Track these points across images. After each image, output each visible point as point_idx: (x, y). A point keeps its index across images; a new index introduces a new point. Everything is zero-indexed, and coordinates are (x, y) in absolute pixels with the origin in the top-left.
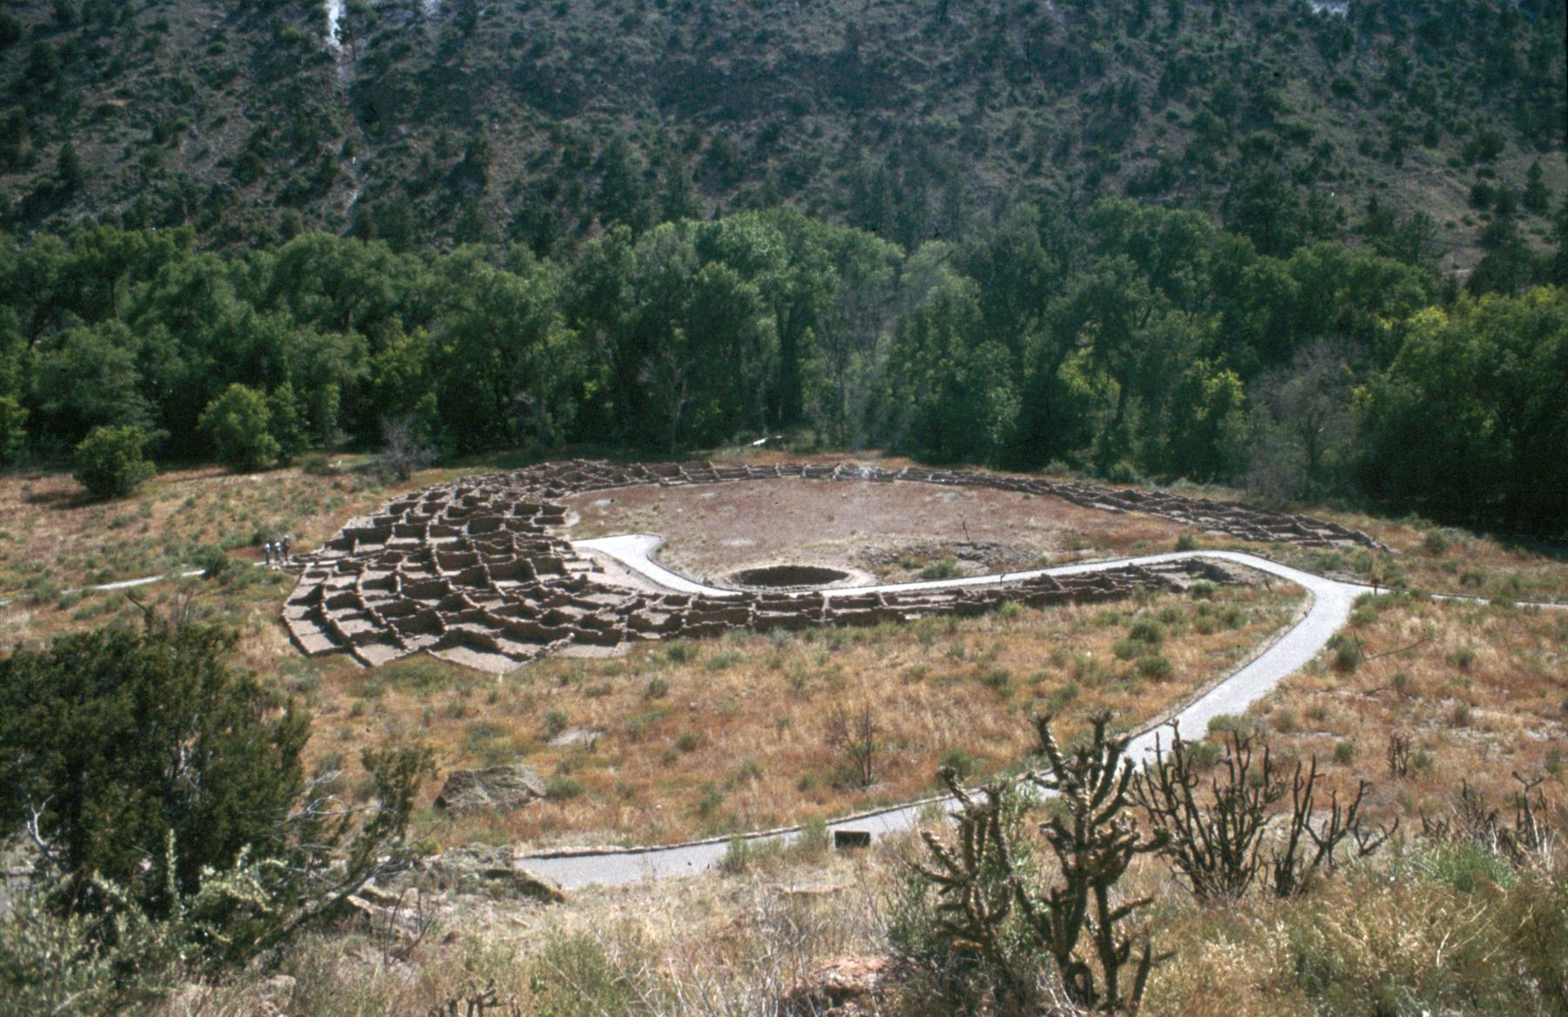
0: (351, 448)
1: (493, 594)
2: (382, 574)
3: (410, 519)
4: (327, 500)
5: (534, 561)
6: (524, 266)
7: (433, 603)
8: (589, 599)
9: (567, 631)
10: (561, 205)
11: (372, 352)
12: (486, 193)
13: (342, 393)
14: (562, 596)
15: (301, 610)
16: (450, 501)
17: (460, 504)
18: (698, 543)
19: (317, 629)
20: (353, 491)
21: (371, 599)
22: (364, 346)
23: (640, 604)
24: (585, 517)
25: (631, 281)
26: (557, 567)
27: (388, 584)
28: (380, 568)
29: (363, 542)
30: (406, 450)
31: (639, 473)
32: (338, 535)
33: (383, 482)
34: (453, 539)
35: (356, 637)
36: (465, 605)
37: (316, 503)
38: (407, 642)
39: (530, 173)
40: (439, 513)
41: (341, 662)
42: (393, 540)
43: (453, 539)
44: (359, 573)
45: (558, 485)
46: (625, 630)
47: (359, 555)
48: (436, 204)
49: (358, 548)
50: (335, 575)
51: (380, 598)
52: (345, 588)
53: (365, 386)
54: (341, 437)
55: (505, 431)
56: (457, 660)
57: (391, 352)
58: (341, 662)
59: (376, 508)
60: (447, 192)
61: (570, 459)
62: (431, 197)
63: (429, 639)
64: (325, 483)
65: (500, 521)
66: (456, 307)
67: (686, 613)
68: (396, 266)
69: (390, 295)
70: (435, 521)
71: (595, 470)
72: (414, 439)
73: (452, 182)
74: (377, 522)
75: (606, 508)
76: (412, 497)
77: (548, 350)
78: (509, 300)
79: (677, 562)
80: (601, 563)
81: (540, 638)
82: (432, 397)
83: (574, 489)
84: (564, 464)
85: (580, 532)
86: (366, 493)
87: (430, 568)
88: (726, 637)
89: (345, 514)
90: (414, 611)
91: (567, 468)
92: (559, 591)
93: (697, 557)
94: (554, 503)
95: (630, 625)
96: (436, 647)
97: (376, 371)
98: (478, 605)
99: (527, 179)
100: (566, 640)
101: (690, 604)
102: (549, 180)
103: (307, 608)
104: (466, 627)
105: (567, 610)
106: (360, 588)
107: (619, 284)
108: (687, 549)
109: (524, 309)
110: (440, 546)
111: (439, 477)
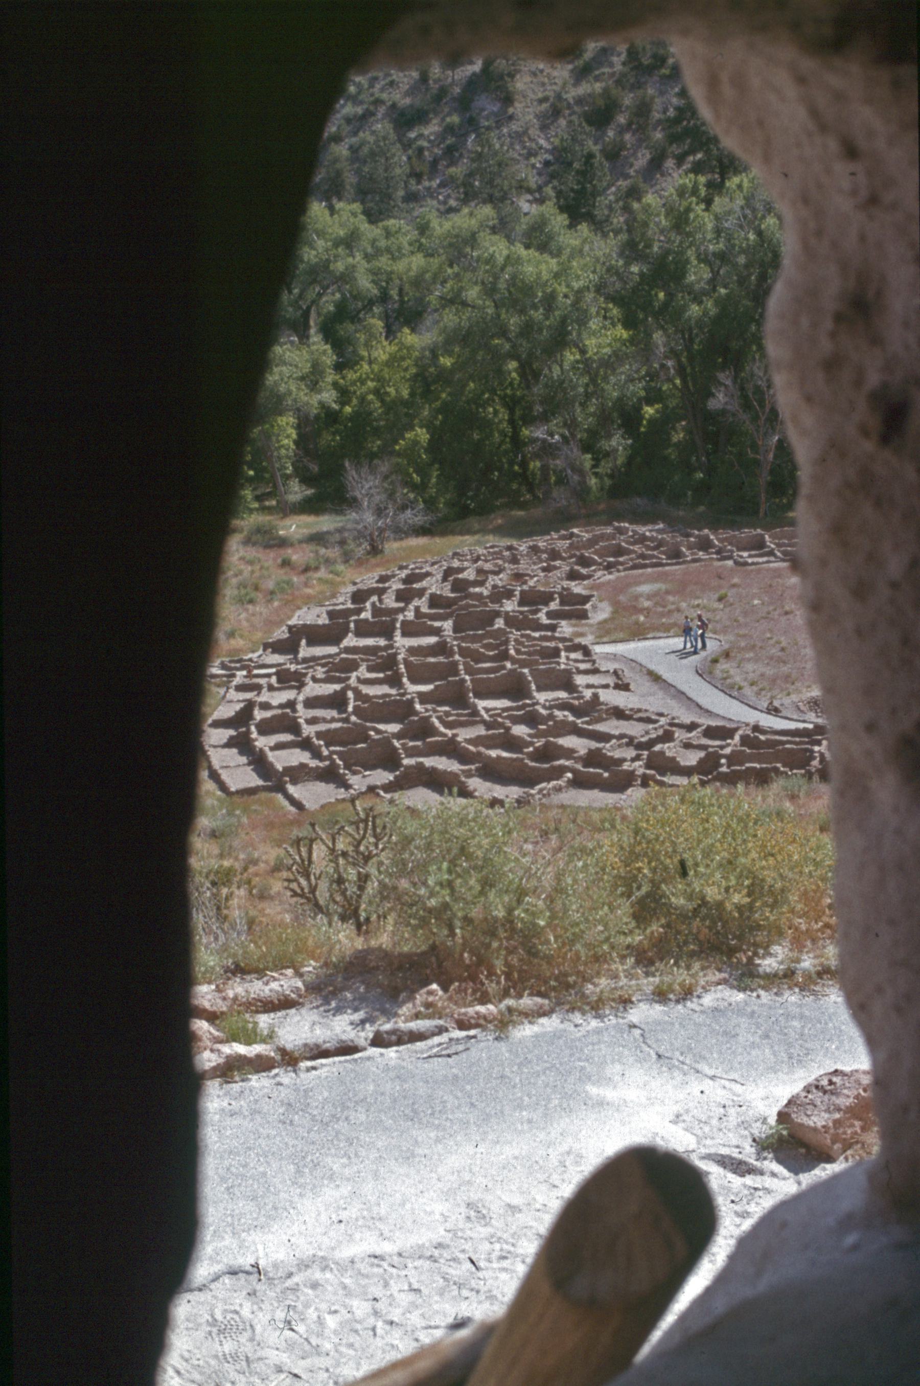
0: (309, 507)
1: (473, 717)
2: (330, 688)
3: (376, 611)
4: (270, 585)
5: (532, 672)
6: (550, 237)
7: (393, 728)
8: (601, 727)
9: (562, 770)
10: (622, 131)
11: (339, 367)
12: (511, 118)
13: (298, 427)
14: (564, 723)
15: (226, 734)
16: (434, 585)
17: (446, 591)
18: (774, 651)
19: (244, 760)
20: (307, 569)
21: (312, 721)
22: (329, 358)
23: (667, 737)
24: (618, 609)
25: (703, 258)
26: (566, 682)
27: (337, 702)
28: (328, 680)
29: (310, 643)
30: (379, 512)
31: (705, 545)
32: (281, 633)
33: (347, 558)
34: (432, 640)
35: (288, 770)
36: (433, 731)
37: (256, 588)
38: (353, 780)
39: (577, 82)
40: (416, 602)
41: (270, 803)
42: (350, 641)
43: (432, 640)
44: (301, 686)
45: (585, 562)
46: (640, 771)
47: (305, 660)
48: (442, 137)
49: (305, 651)
50: (271, 688)
51: (324, 720)
52: (281, 706)
53: (330, 417)
54: (297, 492)
55: (525, 477)
56: (566, 802)
57: (366, 367)
58: (270, 803)
59: (334, 596)
60: (455, 119)
61: (608, 523)
62: (432, 129)
63: (382, 777)
64: (270, 558)
65: (497, 614)
66: (455, 301)
67: (728, 751)
68: (374, 242)
69: (365, 283)
70: (410, 615)
71: (642, 539)
72: (391, 496)
73: (464, 103)
74: (331, 614)
75: (649, 597)
76: (383, 579)
77: (587, 362)
78: (528, 290)
79: (738, 679)
80: (628, 675)
81: (526, 779)
82: (422, 435)
83: (609, 567)
84: (599, 530)
85: (608, 632)
86: (322, 573)
87: (394, 681)
88: (777, 786)
89: (293, 604)
90: (366, 738)
91: (602, 537)
92: (559, 714)
93: (770, 672)
94: (578, 588)
95: (648, 766)
96: (389, 787)
97: (344, 394)
98: (449, 733)
99: (572, 94)
100: (561, 782)
101: (737, 738)
102: (606, 91)
103: (232, 732)
104: (429, 762)
105: (569, 742)
106: (300, 707)
107: (687, 261)
108: (756, 660)
109: (550, 301)
110: (412, 651)
111: (425, 550)
